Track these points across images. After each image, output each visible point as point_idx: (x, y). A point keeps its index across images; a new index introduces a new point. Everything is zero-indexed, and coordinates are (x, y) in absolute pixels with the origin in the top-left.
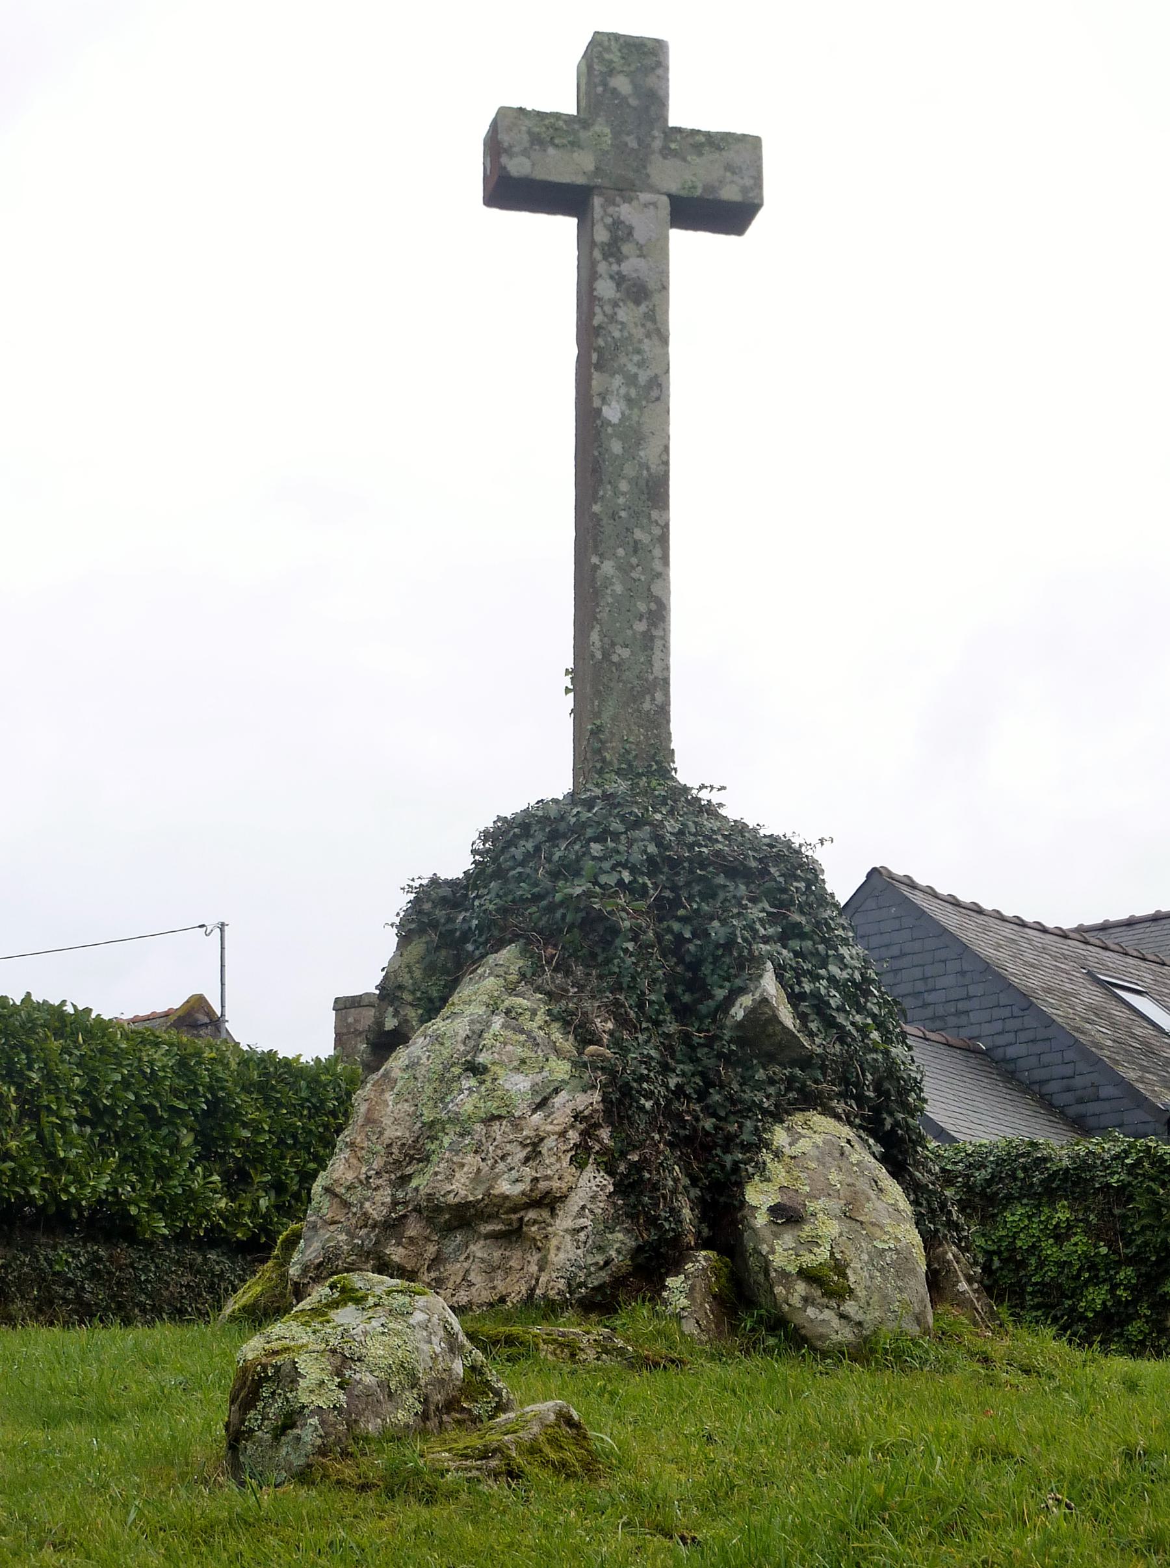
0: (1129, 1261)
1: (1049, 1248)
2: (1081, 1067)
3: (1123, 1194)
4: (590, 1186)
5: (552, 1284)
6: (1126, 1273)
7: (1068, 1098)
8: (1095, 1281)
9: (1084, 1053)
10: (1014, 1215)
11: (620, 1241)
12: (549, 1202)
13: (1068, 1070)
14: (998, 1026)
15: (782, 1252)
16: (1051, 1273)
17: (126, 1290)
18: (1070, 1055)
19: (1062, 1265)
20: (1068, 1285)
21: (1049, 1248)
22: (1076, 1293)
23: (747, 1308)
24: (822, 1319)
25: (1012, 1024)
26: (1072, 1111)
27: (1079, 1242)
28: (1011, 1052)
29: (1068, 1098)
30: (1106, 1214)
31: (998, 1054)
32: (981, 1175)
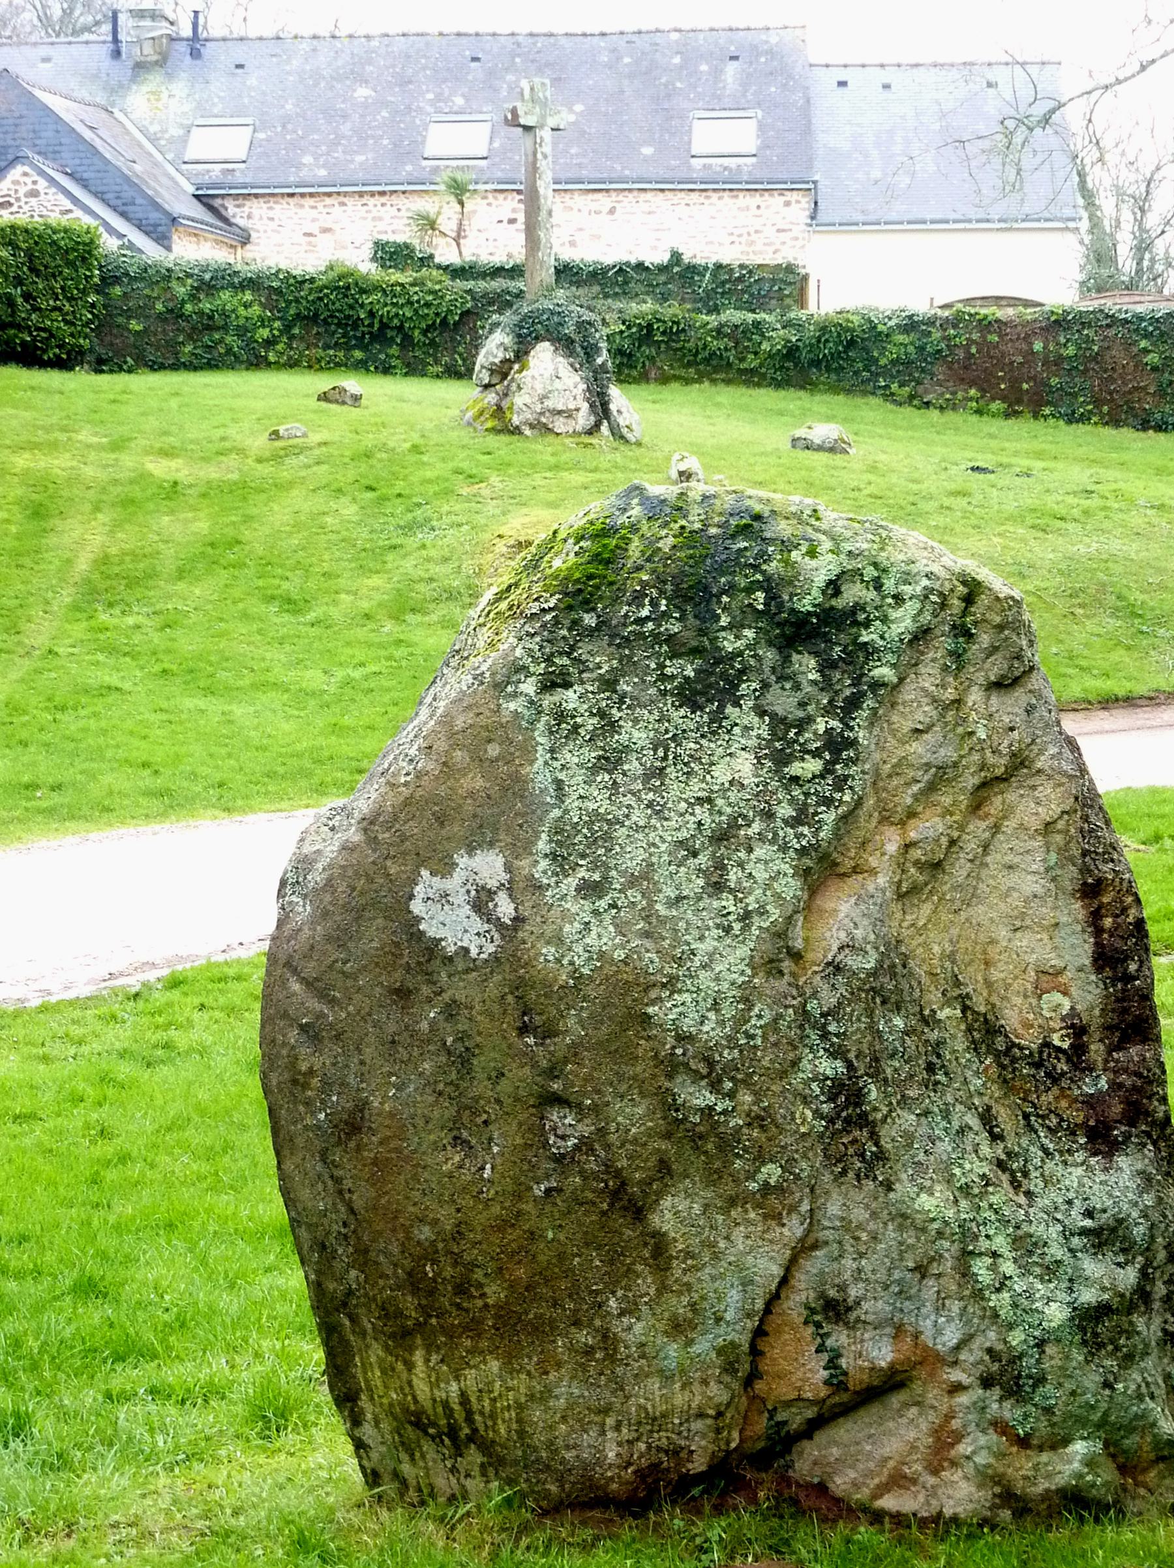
0: (279, 319)
1: (242, 311)
2: (126, 187)
3: (278, 291)
4: (586, 405)
5: (579, 428)
6: (277, 324)
7: (119, 202)
8: (263, 326)
9: (127, 179)
10: (225, 295)
11: (592, 418)
12: (577, 410)
13: (118, 188)
14: (78, 161)
15: (622, 422)
16: (242, 322)
17: (24, 343)
18: (118, 181)
19: (247, 318)
20: (250, 326)
21: (242, 311)
22: (254, 330)
23: (618, 435)
24: (629, 436)
25: (85, 161)
26: (121, 209)
27: (256, 310)
28: (85, 176)
29: (119, 202)
30: (269, 298)
31: (78, 176)
32: (207, 276)
